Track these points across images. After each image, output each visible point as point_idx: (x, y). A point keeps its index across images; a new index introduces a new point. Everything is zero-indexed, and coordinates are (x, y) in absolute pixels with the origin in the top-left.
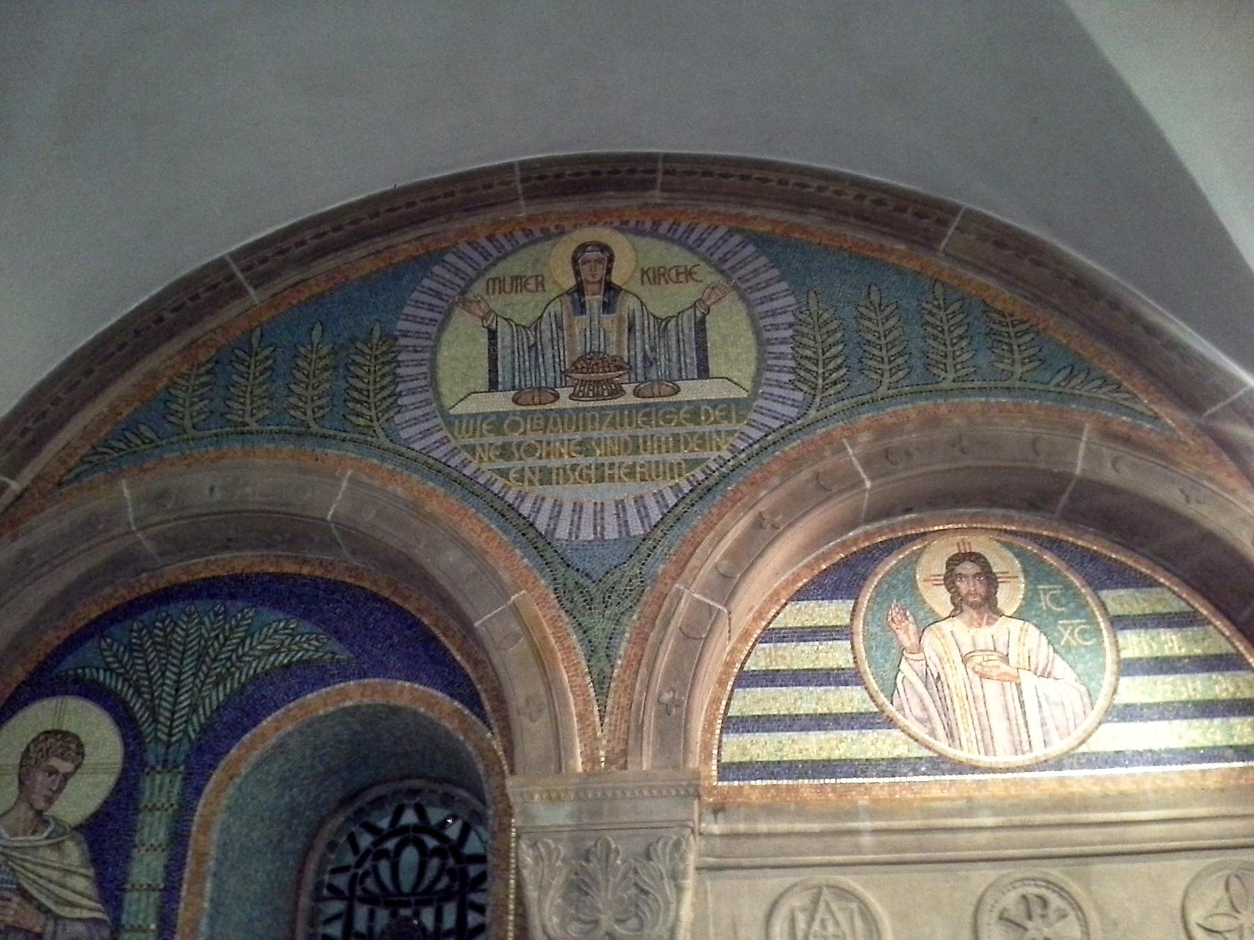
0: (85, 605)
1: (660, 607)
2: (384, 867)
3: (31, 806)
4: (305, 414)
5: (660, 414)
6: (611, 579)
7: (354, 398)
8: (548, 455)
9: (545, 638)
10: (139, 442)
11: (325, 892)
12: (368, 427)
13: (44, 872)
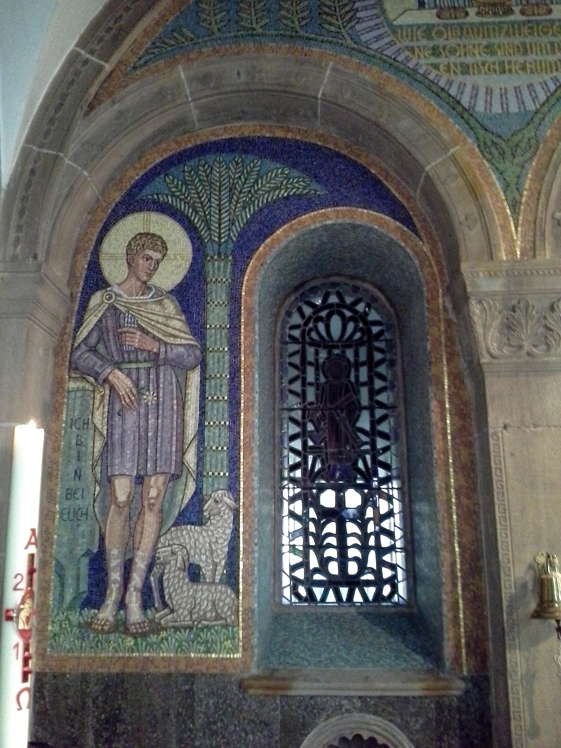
0: (151, 154)
1: (551, 158)
2: (321, 326)
3: (138, 279)
4: (293, 22)
5: (540, 28)
6: (516, 139)
7: (326, 12)
8: (465, 54)
9: (475, 177)
10: (183, 40)
11: (287, 339)
12: (338, 32)
13: (154, 317)
